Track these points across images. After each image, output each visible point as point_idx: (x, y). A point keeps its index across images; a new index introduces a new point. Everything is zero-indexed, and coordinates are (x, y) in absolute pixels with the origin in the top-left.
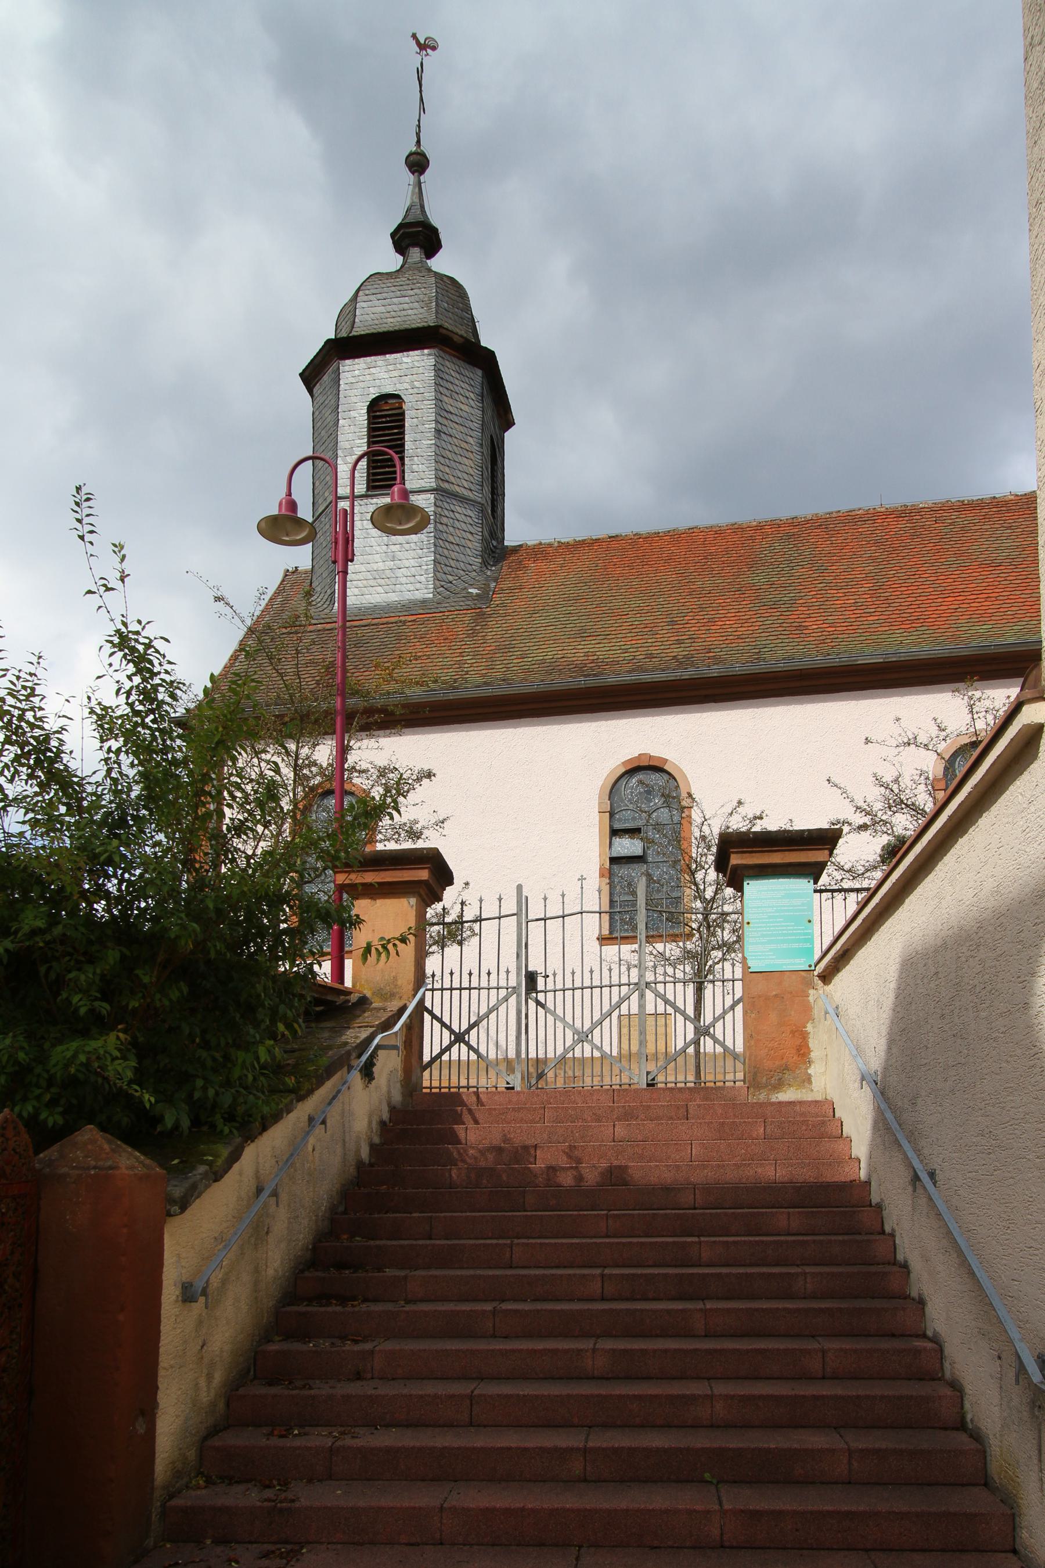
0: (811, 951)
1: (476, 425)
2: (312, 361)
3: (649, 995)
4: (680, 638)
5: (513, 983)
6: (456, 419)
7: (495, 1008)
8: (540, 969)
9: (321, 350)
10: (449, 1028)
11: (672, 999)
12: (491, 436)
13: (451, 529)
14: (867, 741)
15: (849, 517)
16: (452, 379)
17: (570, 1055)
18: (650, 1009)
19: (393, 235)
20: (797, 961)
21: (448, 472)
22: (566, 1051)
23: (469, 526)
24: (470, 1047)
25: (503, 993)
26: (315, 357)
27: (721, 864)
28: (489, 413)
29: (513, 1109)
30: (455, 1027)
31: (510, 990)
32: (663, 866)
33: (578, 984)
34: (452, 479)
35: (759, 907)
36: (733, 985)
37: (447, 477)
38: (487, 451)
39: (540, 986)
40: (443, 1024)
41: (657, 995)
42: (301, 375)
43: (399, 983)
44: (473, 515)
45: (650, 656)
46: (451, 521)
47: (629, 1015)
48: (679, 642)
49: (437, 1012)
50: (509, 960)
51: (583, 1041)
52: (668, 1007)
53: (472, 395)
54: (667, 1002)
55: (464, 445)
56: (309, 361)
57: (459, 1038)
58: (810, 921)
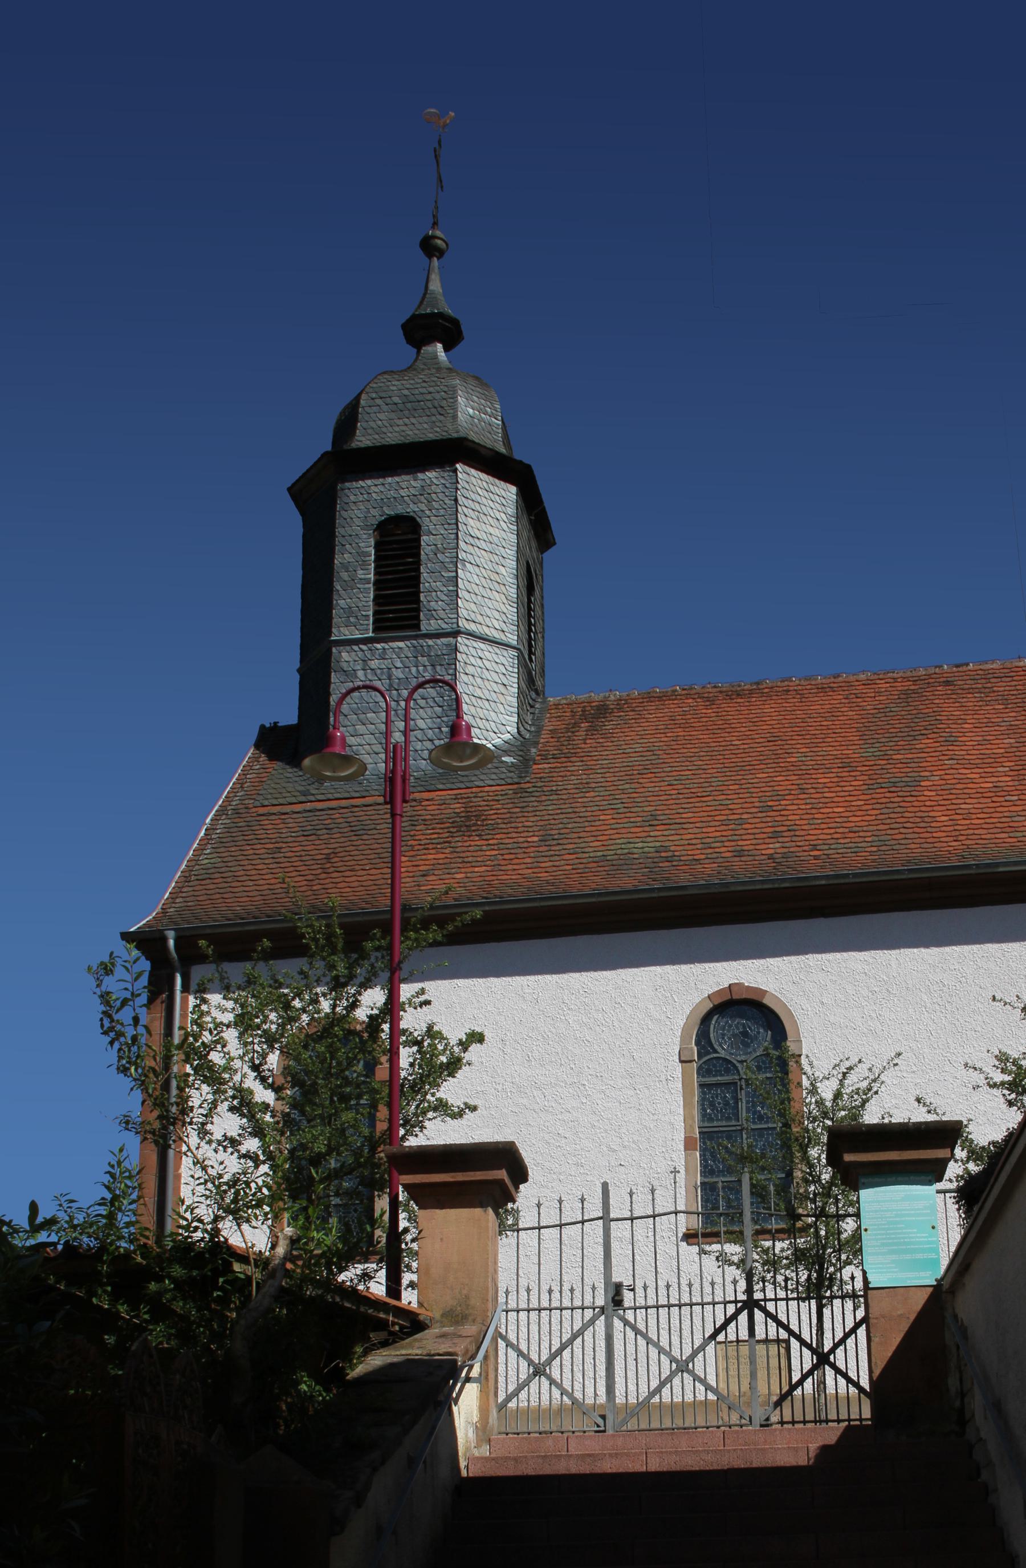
0: (936, 1262)
1: (509, 552)
2: (304, 474)
3: (759, 1315)
4: (777, 829)
5: (600, 1302)
6: (483, 545)
7: (581, 1332)
8: (627, 1282)
9: (316, 463)
10: (526, 1357)
11: (797, 1330)
12: (528, 563)
13: (479, 680)
14: (994, 999)
15: (980, 672)
16: (478, 498)
17: (656, 1399)
18: (760, 1333)
19: (404, 327)
20: (922, 1274)
21: (475, 610)
22: (652, 1394)
23: (501, 676)
24: (552, 1382)
25: (589, 1314)
26: (308, 471)
27: (833, 1160)
28: (525, 534)
29: (610, 1455)
30: (534, 1357)
31: (597, 1310)
32: (768, 1134)
33: (578, 1303)
34: (480, 619)
35: (876, 1211)
36: (583, 1313)
37: (473, 616)
38: (523, 583)
39: (628, 1302)
40: (520, 1353)
41: (768, 1314)
42: (289, 490)
43: (472, 1302)
44: (506, 663)
45: (740, 854)
46: (479, 670)
47: (738, 1341)
48: (776, 835)
49: (512, 1337)
50: (595, 1275)
51: (682, 1371)
52: (781, 1330)
53: (503, 515)
54: (779, 1324)
55: (494, 577)
56: (301, 474)
57: (539, 1371)
58: (933, 1228)
